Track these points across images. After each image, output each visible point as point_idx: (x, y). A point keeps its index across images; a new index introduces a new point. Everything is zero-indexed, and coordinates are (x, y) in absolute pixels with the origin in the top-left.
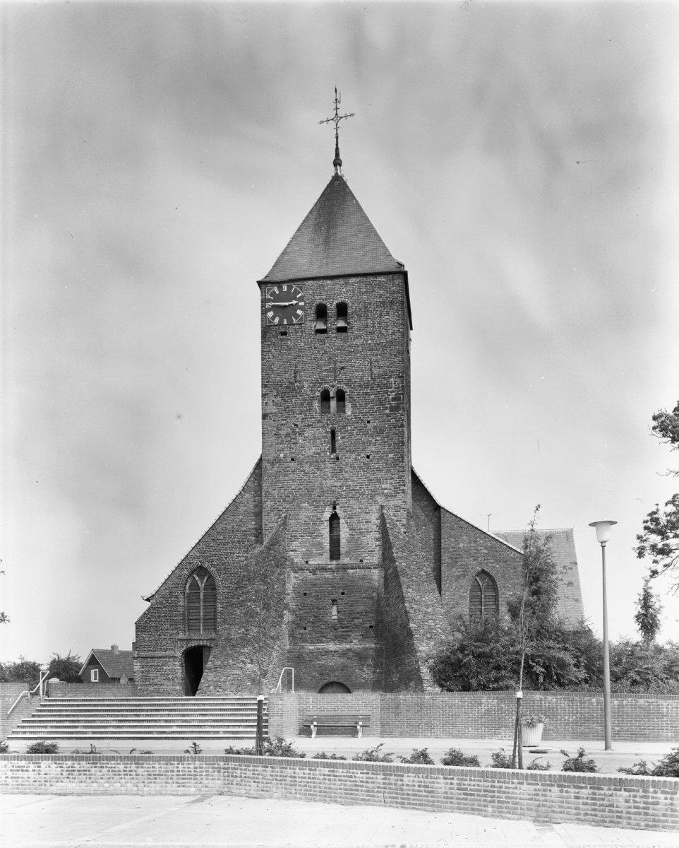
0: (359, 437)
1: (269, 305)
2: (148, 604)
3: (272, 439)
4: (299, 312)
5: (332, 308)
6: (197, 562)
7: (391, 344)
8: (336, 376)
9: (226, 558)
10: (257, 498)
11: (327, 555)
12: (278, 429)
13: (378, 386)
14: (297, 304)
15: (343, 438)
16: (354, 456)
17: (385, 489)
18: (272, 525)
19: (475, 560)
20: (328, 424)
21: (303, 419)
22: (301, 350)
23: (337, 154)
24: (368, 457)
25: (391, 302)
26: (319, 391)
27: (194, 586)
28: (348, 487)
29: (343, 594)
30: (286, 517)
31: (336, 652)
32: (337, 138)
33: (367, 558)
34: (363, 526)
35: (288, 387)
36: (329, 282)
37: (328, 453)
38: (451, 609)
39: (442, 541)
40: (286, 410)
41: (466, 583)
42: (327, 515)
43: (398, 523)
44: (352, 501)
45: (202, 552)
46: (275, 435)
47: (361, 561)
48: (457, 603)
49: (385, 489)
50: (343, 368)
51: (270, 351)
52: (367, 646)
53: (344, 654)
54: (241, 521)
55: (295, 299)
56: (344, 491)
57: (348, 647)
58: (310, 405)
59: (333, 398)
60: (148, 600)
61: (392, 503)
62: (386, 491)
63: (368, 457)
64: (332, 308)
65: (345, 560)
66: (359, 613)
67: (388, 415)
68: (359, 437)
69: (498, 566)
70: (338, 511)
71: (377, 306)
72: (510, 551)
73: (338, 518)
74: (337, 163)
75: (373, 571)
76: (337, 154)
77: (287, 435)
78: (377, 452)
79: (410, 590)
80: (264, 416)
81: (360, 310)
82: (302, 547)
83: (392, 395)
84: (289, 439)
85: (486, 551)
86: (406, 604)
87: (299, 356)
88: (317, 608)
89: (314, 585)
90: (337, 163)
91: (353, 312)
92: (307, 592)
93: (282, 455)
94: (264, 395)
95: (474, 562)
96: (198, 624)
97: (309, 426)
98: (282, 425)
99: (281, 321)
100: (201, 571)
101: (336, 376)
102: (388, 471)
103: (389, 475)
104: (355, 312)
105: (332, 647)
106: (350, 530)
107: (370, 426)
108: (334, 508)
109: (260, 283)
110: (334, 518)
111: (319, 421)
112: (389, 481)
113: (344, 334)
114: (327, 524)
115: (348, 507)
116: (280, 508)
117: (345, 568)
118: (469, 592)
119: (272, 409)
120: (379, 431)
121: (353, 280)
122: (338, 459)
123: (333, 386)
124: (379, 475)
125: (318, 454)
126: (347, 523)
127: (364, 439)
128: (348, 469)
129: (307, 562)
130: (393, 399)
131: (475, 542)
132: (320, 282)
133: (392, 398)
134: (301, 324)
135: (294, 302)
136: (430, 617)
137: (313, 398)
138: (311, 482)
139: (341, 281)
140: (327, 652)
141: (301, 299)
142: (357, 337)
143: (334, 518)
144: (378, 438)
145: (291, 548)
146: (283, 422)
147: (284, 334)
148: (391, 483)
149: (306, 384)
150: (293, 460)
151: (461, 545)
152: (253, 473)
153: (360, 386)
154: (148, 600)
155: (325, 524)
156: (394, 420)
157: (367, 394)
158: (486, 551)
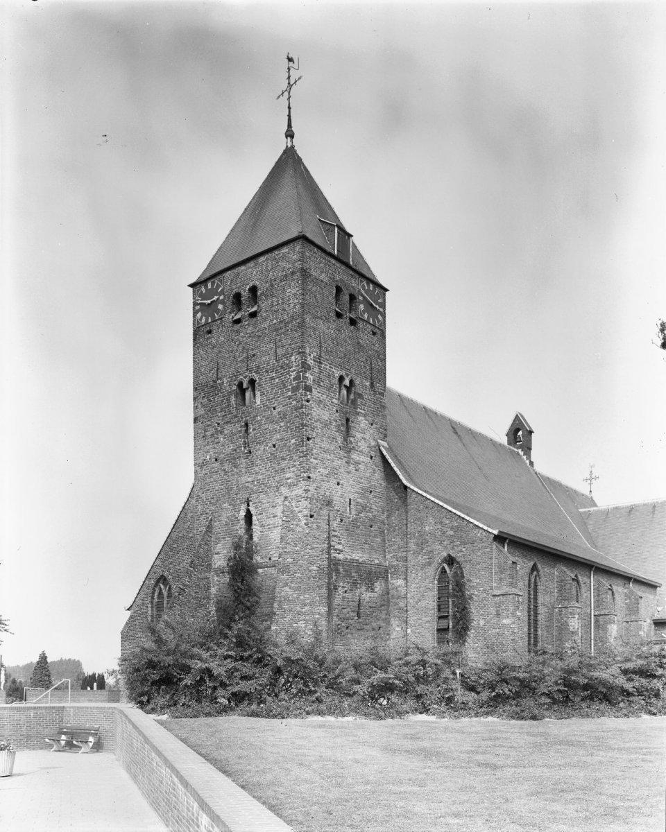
0: (266, 426)
1: (198, 307)
2: (129, 613)
3: (201, 442)
4: (220, 307)
5: (245, 294)
6: (160, 572)
7: (293, 318)
8: (248, 366)
12: (205, 431)
13: (282, 367)
14: (218, 299)
15: (254, 430)
17: (288, 479)
19: (441, 544)
20: (242, 418)
21: (224, 416)
22: (222, 345)
23: (290, 125)
25: (293, 273)
26: (235, 384)
27: (444, 571)
28: (258, 481)
30: (211, 520)
32: (289, 108)
33: (275, 555)
34: (271, 521)
35: (212, 387)
36: (243, 268)
37: (243, 448)
38: (417, 603)
40: (211, 410)
41: (432, 572)
42: (243, 513)
43: (299, 515)
44: (262, 496)
45: (163, 561)
46: (203, 437)
47: (270, 559)
48: (423, 596)
49: (288, 479)
50: (254, 355)
51: (199, 353)
55: (217, 294)
56: (254, 486)
58: (228, 400)
59: (247, 388)
60: (128, 609)
61: (294, 493)
62: (289, 481)
63: (274, 446)
64: (245, 294)
66: (266, 615)
67: (290, 398)
68: (266, 426)
69: (464, 549)
70: (251, 508)
71: (281, 281)
72: (477, 530)
74: (290, 134)
76: (290, 125)
77: (212, 435)
78: (281, 440)
79: (286, 589)
80: (195, 420)
81: (267, 289)
83: (294, 375)
84: (213, 439)
85: (452, 533)
86: (276, 605)
87: (220, 352)
90: (290, 134)
91: (261, 294)
93: (208, 457)
94: (195, 399)
95: (440, 547)
96: (447, 610)
97: (228, 422)
98: (208, 426)
99: (207, 319)
100: (163, 579)
101: (248, 366)
102: (291, 459)
103: (292, 462)
104: (263, 294)
107: (275, 413)
108: (248, 505)
109: (192, 286)
110: (249, 517)
111: (236, 416)
112: (292, 469)
113: (255, 319)
114: (242, 522)
115: (259, 502)
118: (436, 582)
119: (201, 411)
120: (283, 416)
121: (262, 259)
122: (250, 452)
123: (245, 377)
124: (284, 464)
125: (235, 450)
127: (271, 427)
128: (258, 462)
130: (294, 379)
131: (441, 523)
132: (236, 271)
133: (294, 378)
134: (222, 318)
135: (216, 298)
136: (302, 618)
137: (229, 394)
138: (229, 481)
139: (251, 264)
141: (222, 293)
142: (265, 319)
143: (249, 517)
144: (282, 424)
145: (216, 551)
146: (209, 423)
147: (210, 332)
149: (225, 380)
150: (216, 460)
151: (427, 528)
152: (384, 467)
153: (267, 372)
154: (128, 609)
156: (295, 402)
157: (272, 378)
158: (452, 533)
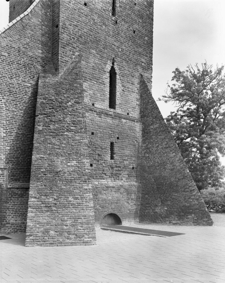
9: (11, 78)
10: (44, 27)
11: (107, 103)
16: (126, 25)
18: (67, 59)
24: (134, 32)
29: (118, 138)
31: (113, 187)
39: (36, 136)
42: (108, 68)
52: (132, 183)
53: (118, 189)
54: (27, 44)
57: (121, 183)
62: (143, 64)
65: (118, 110)
73: (115, 74)
75: (136, 124)
82: (91, 89)
88: (101, 148)
89: (100, 127)
92: (95, 132)
105: (110, 182)
106: (123, 86)
116: (75, 45)
117: (119, 117)
124: (140, 50)
126: (121, 80)
129: (93, 105)
140: (107, 187)
143: (113, 74)
148: (146, 60)
155: (107, 75)
